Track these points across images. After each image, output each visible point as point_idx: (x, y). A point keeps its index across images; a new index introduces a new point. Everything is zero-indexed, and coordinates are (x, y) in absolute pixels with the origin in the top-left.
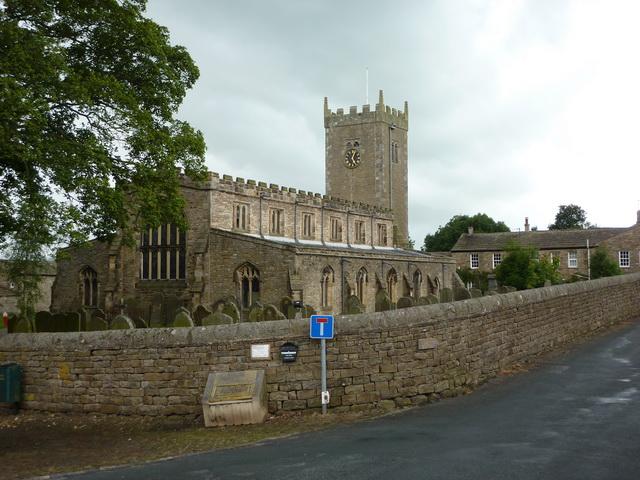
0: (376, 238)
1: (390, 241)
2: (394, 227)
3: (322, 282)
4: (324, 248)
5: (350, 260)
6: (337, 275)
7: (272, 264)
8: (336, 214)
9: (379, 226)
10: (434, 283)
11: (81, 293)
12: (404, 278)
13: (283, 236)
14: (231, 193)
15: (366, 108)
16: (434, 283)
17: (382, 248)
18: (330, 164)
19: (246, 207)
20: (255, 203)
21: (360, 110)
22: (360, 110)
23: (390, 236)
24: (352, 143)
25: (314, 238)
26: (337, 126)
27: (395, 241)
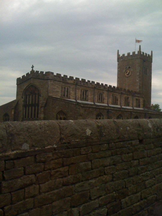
0: (135, 104)
1: (141, 106)
2: (144, 101)
4: (121, 108)
5: (113, 111)
9: (137, 99)
13: (88, 101)
14: (60, 82)
15: (134, 53)
17: (114, 106)
19: (69, 88)
20: (73, 86)
21: (131, 54)
23: (141, 104)
24: (128, 67)
25: (103, 103)
26: (122, 61)
27: (144, 106)
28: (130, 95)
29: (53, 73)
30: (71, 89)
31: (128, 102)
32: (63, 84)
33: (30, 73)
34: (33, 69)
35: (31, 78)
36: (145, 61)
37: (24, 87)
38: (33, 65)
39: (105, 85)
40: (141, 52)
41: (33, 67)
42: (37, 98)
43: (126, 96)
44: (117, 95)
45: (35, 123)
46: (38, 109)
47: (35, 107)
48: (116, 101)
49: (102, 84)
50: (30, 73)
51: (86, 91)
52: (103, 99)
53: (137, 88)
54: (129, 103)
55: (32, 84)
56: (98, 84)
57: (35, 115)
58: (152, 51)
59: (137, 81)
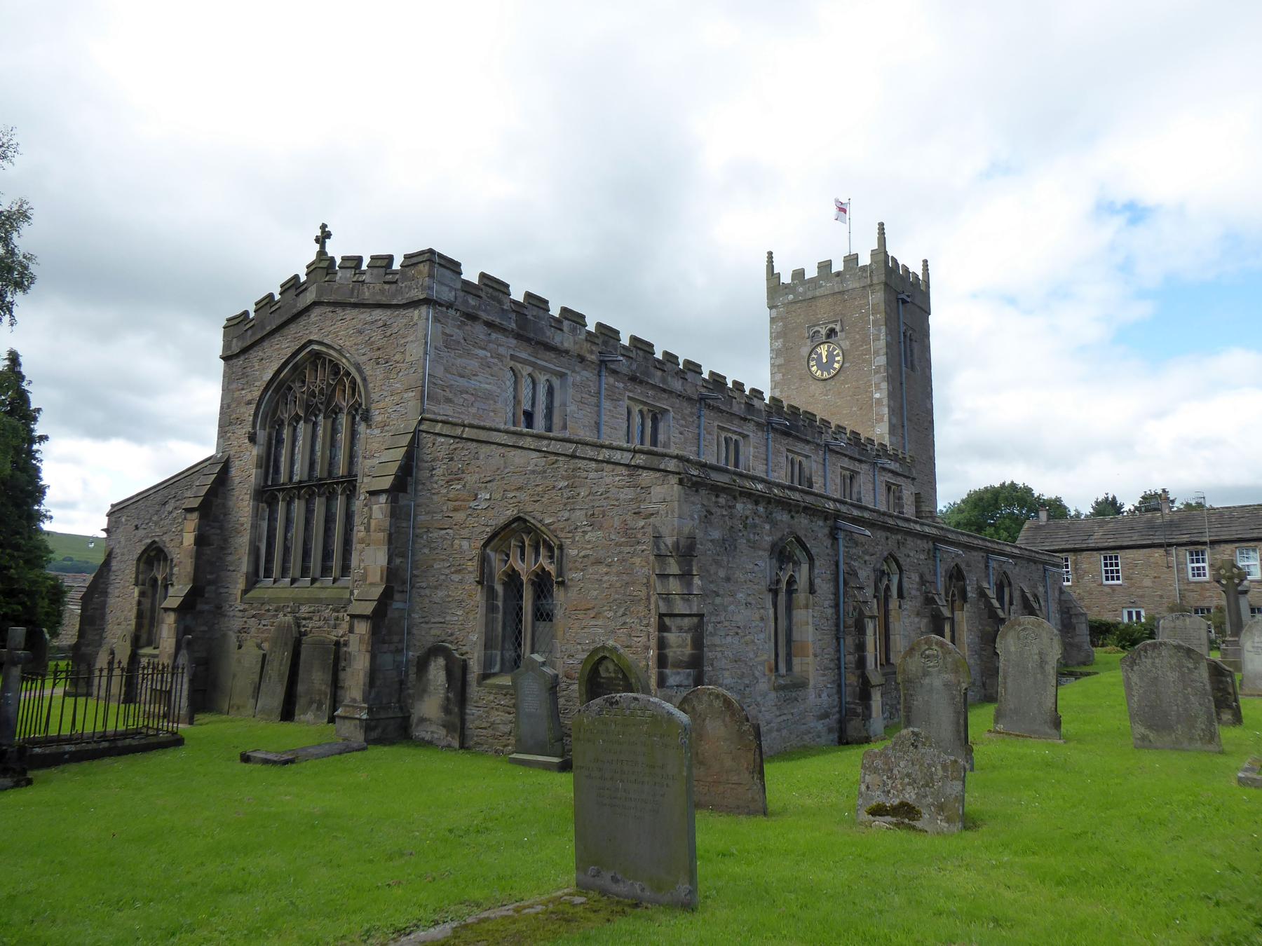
2: (918, 496)
3: (775, 593)
6: (823, 568)
7: (594, 521)
11: (140, 615)
12: (982, 594)
15: (851, 260)
18: (779, 377)
19: (556, 382)
20: (585, 375)
21: (812, 273)
22: (838, 266)
24: (824, 332)
26: (791, 303)
28: (860, 461)
30: (571, 391)
32: (524, 355)
33: (303, 278)
34: (322, 252)
35: (315, 304)
36: (904, 302)
37: (269, 362)
38: (324, 227)
39: (753, 390)
40: (886, 252)
41: (324, 236)
42: (342, 437)
43: (846, 463)
44: (807, 457)
45: (877, 353)
46: (349, 516)
47: (331, 498)
50: (303, 278)
51: (656, 416)
53: (878, 431)
55: (316, 347)
56: (717, 381)
57: (327, 555)
58: (925, 262)
59: (877, 396)
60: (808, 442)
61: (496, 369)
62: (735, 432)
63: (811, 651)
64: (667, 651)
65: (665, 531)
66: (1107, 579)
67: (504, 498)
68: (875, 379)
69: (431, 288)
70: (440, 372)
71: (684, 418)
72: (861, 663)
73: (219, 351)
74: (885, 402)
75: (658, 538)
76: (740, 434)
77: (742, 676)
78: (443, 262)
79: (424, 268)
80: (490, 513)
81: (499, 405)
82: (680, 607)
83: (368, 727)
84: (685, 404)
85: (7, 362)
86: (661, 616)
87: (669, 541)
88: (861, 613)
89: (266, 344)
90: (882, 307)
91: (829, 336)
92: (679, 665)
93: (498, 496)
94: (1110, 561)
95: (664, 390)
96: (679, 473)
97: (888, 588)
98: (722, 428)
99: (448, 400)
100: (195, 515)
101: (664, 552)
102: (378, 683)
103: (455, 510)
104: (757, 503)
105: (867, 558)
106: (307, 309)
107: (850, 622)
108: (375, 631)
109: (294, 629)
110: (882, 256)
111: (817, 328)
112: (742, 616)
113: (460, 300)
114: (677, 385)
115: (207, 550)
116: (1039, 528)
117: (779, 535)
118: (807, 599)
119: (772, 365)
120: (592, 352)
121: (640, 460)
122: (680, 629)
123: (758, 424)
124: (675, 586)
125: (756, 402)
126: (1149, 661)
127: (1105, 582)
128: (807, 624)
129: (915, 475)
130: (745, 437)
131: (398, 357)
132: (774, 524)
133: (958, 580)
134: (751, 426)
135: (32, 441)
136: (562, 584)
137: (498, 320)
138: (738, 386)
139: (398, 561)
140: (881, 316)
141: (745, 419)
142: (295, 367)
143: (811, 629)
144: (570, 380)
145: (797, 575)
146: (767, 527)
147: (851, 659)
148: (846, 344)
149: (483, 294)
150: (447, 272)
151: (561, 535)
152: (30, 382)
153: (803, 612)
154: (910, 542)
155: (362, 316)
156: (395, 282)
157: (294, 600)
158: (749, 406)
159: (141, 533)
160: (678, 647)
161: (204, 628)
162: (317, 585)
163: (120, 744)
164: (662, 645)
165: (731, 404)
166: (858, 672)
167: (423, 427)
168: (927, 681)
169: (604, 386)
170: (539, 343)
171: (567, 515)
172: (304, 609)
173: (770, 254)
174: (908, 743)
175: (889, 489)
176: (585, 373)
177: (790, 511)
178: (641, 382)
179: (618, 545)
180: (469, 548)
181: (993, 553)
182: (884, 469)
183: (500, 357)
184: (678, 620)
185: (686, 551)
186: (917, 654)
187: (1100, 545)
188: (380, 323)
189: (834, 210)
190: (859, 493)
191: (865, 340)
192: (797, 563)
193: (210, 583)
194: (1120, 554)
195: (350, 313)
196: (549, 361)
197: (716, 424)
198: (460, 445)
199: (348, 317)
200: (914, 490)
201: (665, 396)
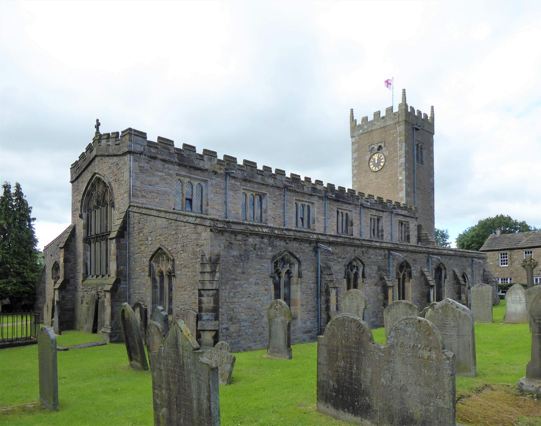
2: (419, 228)
8: (345, 206)
9: (401, 223)
10: (461, 278)
12: (423, 274)
15: (390, 110)
16: (461, 278)
18: (356, 171)
19: (203, 184)
21: (371, 118)
23: (413, 234)
24: (376, 148)
26: (361, 134)
28: (383, 211)
29: (143, 135)
30: (210, 188)
31: (380, 229)
34: (98, 132)
35: (96, 156)
36: (417, 129)
38: (98, 120)
39: (317, 181)
40: (406, 106)
41: (98, 125)
43: (374, 212)
44: (350, 211)
45: (400, 156)
48: (349, 228)
49: (306, 178)
51: (261, 197)
52: (311, 222)
53: (401, 195)
54: (382, 231)
59: (400, 178)
60: (350, 204)
61: (168, 181)
62: (306, 202)
63: (299, 303)
64: (202, 305)
65: (206, 253)
66: (502, 264)
67: (156, 239)
68: (399, 170)
69: (130, 146)
70: (138, 184)
71: (275, 197)
72: (328, 308)
73: (69, 179)
74: (404, 181)
75: (203, 256)
76: (309, 202)
77: (253, 315)
78: (136, 133)
79: (127, 137)
80: (152, 246)
81: (171, 197)
82: (208, 286)
83: (111, 336)
84: (276, 190)
85: (15, 188)
86: (199, 290)
87: (207, 257)
88: (327, 286)
89: (83, 175)
90: (403, 133)
91: (379, 149)
92: (207, 311)
93: (154, 239)
94: (504, 256)
95: (263, 184)
96: (210, 227)
97: (356, 274)
98: (299, 200)
99: (143, 196)
100: (63, 250)
101: (205, 261)
102: (115, 318)
103: (141, 245)
104: (262, 238)
105: (340, 260)
106: (94, 159)
107: (323, 290)
108: (112, 297)
109: (96, 296)
110: (404, 107)
111: (373, 146)
112: (253, 289)
113: (146, 150)
114: (271, 181)
115: (69, 264)
116: (495, 238)
117: (278, 252)
118: (298, 280)
119: (353, 166)
120: (221, 169)
121: (198, 221)
122: (208, 295)
123: (319, 197)
124: (207, 277)
125: (318, 187)
126: (394, 310)
127: (501, 266)
128: (297, 291)
129: (417, 216)
130: (313, 203)
131: (121, 179)
132: (274, 246)
133: (407, 268)
134: (316, 198)
135: (30, 220)
136: (174, 276)
137: (168, 158)
138: (308, 180)
139: (122, 267)
140: (403, 138)
141: (312, 195)
142: (93, 185)
143: (299, 293)
144: (210, 183)
145: (292, 270)
146: (270, 248)
147: (324, 306)
148: (386, 153)
149: (159, 147)
150: (139, 138)
151: (174, 255)
152: (25, 196)
153: (295, 286)
154: (371, 251)
155: (111, 161)
156: (119, 144)
157: (96, 284)
158: (314, 189)
159: (53, 257)
160: (208, 303)
161: (71, 296)
162: (104, 278)
163: (14, 343)
164: (200, 302)
165: (303, 189)
166: (326, 312)
167: (130, 209)
168: (276, 320)
169: (228, 184)
170: (191, 167)
171: (175, 246)
172: (99, 288)
173: (352, 110)
174: (219, 347)
175: (402, 224)
176: (218, 179)
177: (285, 241)
178: (250, 181)
179: (191, 259)
180: (146, 261)
181: (433, 254)
182: (398, 214)
183: (170, 175)
184: (207, 292)
185: (215, 262)
186: (273, 308)
187: (523, 246)
188: (116, 164)
189: (384, 85)
190: (382, 227)
191: (395, 151)
192: (291, 264)
193: (72, 278)
194: (533, 250)
195: (107, 159)
196: (199, 175)
197: (294, 198)
198: (141, 217)
199: (106, 161)
200: (416, 223)
201: (265, 187)
